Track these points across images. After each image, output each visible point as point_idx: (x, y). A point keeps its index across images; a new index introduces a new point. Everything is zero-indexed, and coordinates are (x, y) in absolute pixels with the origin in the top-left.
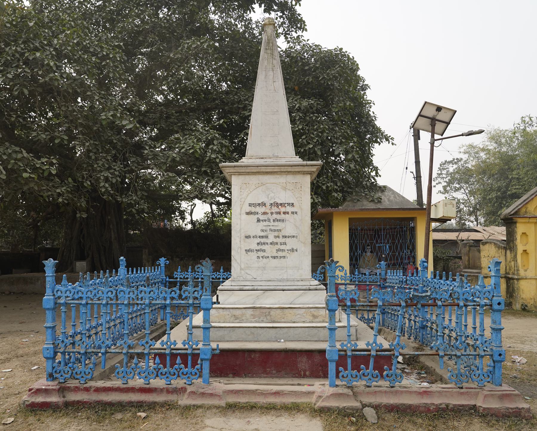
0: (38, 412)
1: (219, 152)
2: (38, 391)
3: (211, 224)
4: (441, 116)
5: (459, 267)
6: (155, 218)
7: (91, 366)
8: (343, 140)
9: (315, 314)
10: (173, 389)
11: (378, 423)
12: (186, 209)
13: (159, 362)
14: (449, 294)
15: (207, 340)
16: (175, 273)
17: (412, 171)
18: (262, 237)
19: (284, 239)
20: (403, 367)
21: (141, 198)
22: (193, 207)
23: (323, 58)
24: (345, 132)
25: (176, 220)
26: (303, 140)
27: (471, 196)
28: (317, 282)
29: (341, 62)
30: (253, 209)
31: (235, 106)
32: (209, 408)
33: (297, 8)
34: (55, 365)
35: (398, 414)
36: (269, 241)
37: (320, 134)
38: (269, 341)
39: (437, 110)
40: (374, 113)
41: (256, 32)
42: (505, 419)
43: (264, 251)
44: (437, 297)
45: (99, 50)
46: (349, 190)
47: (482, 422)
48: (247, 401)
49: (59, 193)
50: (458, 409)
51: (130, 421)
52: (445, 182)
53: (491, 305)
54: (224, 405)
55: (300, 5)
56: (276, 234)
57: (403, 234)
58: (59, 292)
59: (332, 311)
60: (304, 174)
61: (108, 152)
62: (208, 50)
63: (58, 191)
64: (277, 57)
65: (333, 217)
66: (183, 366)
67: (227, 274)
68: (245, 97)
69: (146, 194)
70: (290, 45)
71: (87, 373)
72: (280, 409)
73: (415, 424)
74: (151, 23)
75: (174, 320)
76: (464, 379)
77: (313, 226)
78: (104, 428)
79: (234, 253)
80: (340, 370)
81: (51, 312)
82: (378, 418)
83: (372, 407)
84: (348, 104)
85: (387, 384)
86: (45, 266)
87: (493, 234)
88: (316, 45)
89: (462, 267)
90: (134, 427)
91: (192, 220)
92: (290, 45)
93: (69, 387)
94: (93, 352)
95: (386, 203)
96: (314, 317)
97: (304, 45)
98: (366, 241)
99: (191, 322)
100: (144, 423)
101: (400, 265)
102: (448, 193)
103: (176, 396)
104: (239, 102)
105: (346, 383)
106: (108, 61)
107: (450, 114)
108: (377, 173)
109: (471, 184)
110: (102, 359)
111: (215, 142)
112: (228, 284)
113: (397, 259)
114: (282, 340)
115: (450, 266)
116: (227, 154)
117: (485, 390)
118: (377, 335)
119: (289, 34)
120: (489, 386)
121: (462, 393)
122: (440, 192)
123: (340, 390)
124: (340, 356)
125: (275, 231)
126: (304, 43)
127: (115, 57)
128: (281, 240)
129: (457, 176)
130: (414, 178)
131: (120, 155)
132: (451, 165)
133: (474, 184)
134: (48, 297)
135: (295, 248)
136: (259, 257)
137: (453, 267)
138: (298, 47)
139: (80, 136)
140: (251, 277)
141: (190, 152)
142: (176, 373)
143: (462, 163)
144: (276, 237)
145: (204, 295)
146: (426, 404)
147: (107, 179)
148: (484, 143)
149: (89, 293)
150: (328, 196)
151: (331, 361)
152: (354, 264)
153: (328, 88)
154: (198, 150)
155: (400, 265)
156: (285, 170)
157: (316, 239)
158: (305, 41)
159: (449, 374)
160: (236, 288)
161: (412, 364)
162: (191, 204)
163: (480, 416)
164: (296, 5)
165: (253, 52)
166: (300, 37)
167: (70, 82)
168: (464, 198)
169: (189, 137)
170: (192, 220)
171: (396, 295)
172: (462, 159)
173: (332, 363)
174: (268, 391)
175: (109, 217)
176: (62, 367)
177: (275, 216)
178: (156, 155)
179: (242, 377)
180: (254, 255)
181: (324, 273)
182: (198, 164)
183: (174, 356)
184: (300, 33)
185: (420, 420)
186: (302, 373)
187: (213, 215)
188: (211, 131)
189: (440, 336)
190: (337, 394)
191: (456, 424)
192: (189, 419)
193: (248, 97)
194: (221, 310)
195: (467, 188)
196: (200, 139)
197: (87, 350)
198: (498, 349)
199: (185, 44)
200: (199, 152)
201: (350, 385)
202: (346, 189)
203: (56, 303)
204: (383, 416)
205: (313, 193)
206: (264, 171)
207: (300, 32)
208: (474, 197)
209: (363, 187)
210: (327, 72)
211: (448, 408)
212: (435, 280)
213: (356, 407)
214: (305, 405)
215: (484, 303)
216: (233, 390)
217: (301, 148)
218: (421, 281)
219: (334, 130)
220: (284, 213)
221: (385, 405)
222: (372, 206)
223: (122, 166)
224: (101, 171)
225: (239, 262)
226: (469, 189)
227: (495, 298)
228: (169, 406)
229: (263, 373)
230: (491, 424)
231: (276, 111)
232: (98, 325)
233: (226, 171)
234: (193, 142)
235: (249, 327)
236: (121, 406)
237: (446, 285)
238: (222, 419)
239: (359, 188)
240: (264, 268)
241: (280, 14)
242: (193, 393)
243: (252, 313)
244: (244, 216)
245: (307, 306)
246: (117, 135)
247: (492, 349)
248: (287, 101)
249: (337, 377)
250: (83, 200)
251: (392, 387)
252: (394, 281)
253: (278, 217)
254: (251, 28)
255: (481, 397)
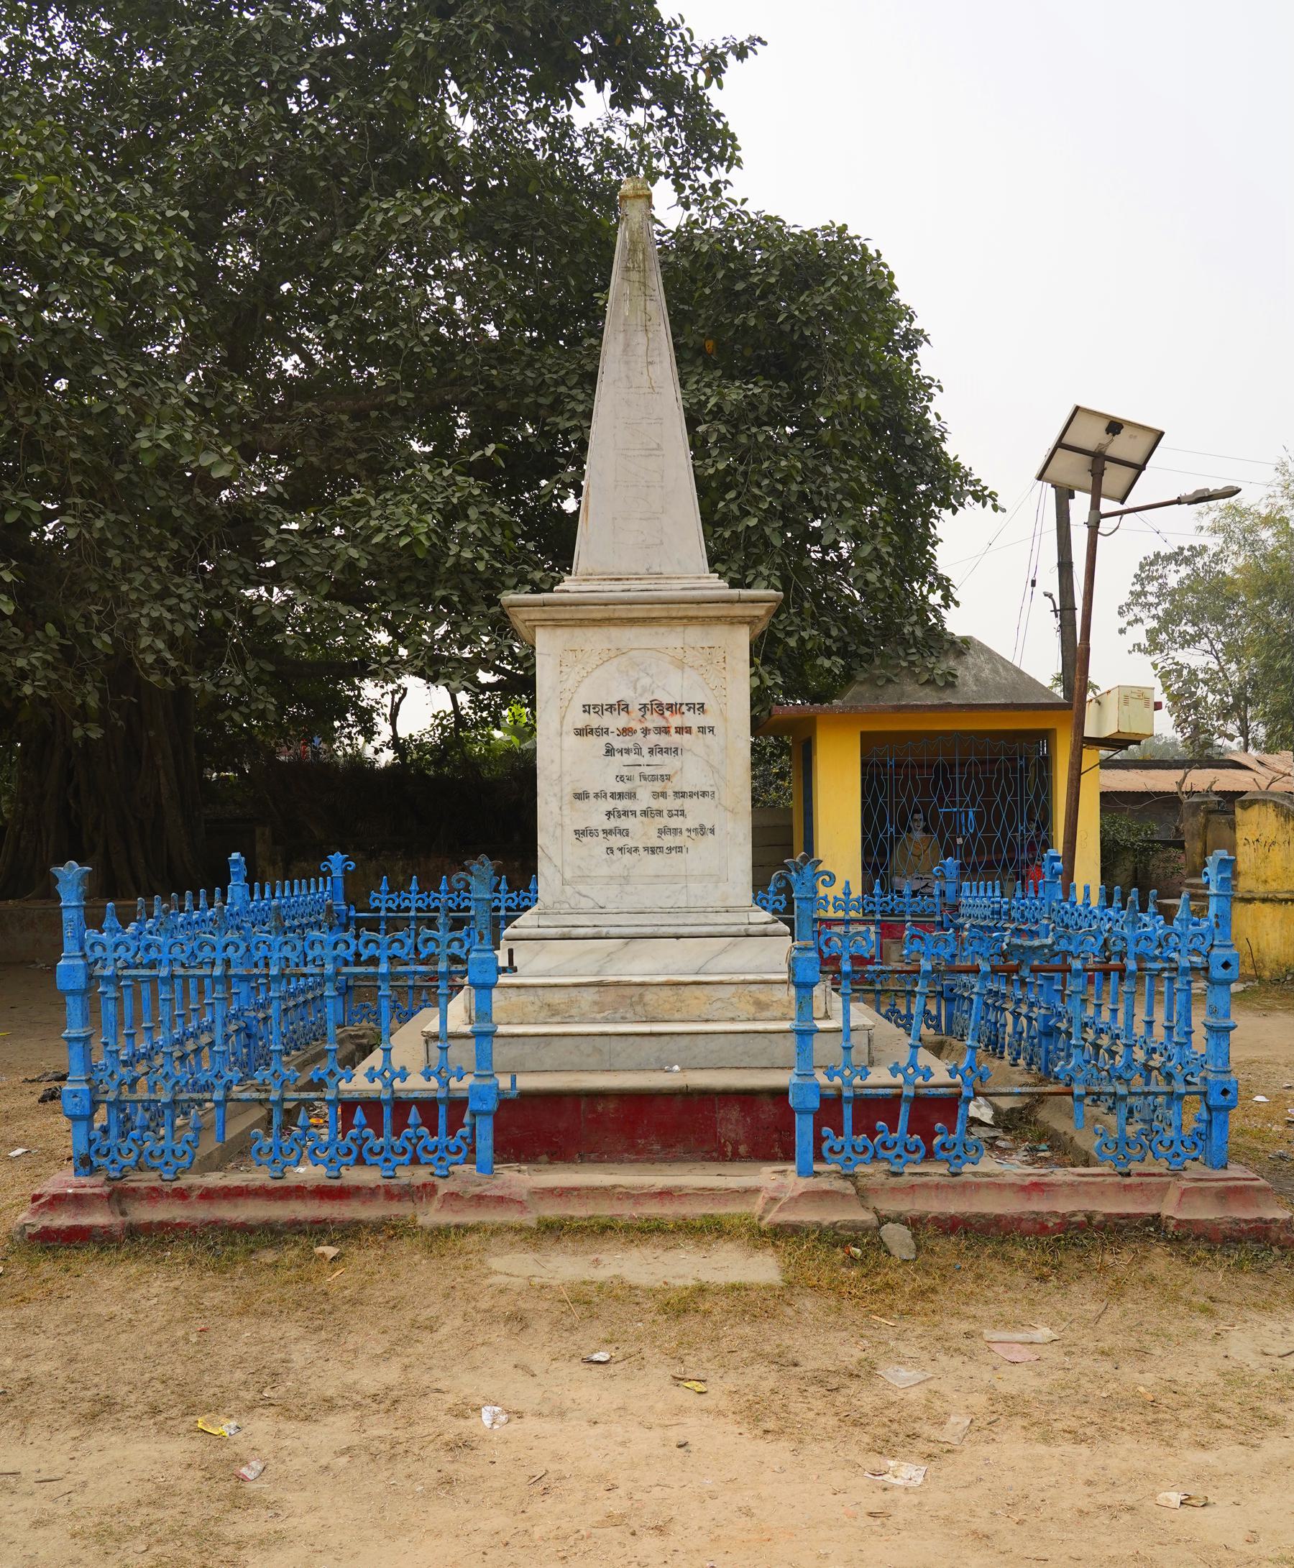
0: (61, 1252)
1: (484, 541)
2: (57, 1201)
3: (452, 748)
4: (1122, 447)
5: (1177, 870)
6: (283, 732)
7: (190, 1135)
8: (847, 504)
9: (762, 997)
10: (403, 1187)
11: (915, 1259)
12: (377, 703)
13: (364, 1121)
14: (1101, 942)
15: (484, 1064)
16: (374, 894)
17: (1049, 591)
18: (621, 795)
19: (679, 801)
20: (992, 1134)
21: (258, 681)
22: (397, 697)
23: (790, 258)
24: (851, 479)
25: (349, 736)
26: (728, 503)
27: (1228, 662)
28: (766, 916)
29: (841, 268)
30: (594, 721)
31: (528, 400)
32: (496, 1231)
33: (712, 93)
34: (96, 1133)
35: (967, 1239)
36: (638, 806)
37: (780, 487)
38: (640, 1069)
39: (1108, 430)
40: (938, 417)
41: (587, 162)
42: (1229, 1248)
43: (624, 833)
44: (1071, 948)
45: (122, 238)
46: (864, 650)
47: (1171, 1255)
48: (590, 1213)
49: (21, 669)
50: (1116, 1224)
51: (299, 1266)
52: (1153, 617)
53: (1206, 969)
54: (533, 1224)
55: (720, 86)
56: (658, 786)
57: (1015, 779)
58: (98, 949)
59: (804, 987)
60: (732, 623)
61: (159, 546)
62: (447, 232)
63: (21, 663)
64: (657, 293)
65: (814, 731)
66: (424, 1130)
67: (399, 896)
68: (556, 372)
69: (271, 668)
70: (691, 215)
71: (178, 1153)
72: (673, 1232)
73: (1008, 1260)
74: (270, 146)
75: (372, 1024)
76: (1135, 1152)
77: (759, 752)
78: (235, 1284)
79: (543, 839)
80: (824, 1134)
81: (79, 999)
82: (918, 1248)
83: (905, 1223)
84: (861, 395)
85: (943, 1169)
86: (57, 881)
87: (1285, 775)
88: (768, 219)
89: (1184, 872)
90: (309, 1280)
91: (395, 736)
92: (691, 215)
93: (134, 1190)
94: (192, 1100)
95: (969, 689)
96: (760, 1005)
97: (731, 215)
98: (910, 799)
99: (443, 1022)
100: (334, 1270)
101: (1005, 868)
102: (1162, 651)
103: (411, 1204)
104: (540, 388)
105: (839, 1168)
106: (150, 272)
107: (1145, 441)
108: (947, 597)
109: (1232, 625)
110: (217, 1114)
111: (473, 513)
112: (530, 923)
113: (999, 850)
114: (676, 1068)
115: (1150, 868)
116: (508, 545)
117: (1184, 1179)
118: (917, 1047)
119: (687, 177)
120: (1195, 1169)
121: (1127, 1188)
122: (1138, 647)
123: (823, 1184)
124: (824, 1100)
125: (654, 778)
126: (734, 209)
127: (169, 258)
128: (671, 803)
129: (1190, 599)
130: (1055, 611)
131: (191, 552)
132: (1173, 567)
133: (1239, 623)
134: (71, 962)
135: (708, 826)
136: (611, 849)
137: (1160, 871)
138: (716, 222)
139: (78, 501)
140: (591, 904)
141: (401, 544)
142: (410, 1148)
143: (1206, 559)
144: (656, 795)
145: (476, 950)
146: (1037, 1213)
147: (157, 627)
148: (1271, 500)
149: (176, 950)
150: (802, 666)
151: (804, 1112)
152: (875, 864)
153: (804, 345)
154: (423, 538)
155: (1005, 868)
156: (681, 614)
157: (766, 791)
158: (735, 203)
159: (1098, 1141)
160: (552, 932)
161: (1016, 1128)
162: (391, 687)
163: (1169, 1241)
164: (708, 84)
165: (578, 235)
166: (721, 186)
167: (41, 338)
168: (1210, 665)
169: (395, 495)
170: (395, 736)
171: (966, 945)
172: (1205, 549)
173: (803, 1116)
174: (642, 1188)
175: (152, 733)
176: (113, 1140)
177: (653, 739)
178: (300, 553)
179: (574, 1162)
180: (597, 846)
181: (788, 890)
182: (422, 578)
183: (401, 1106)
184: (719, 173)
185: (1022, 1253)
186: (729, 1148)
187: (460, 720)
188: (458, 478)
189: (1076, 1046)
190: (818, 1192)
191: (1109, 1259)
192: (447, 1259)
193: (567, 373)
194: (512, 992)
195: (1218, 635)
196: (427, 502)
197: (175, 1094)
198: (1221, 1077)
199: (376, 212)
200: (427, 544)
201: (850, 1172)
202: (854, 647)
203: (90, 977)
204: (930, 1243)
205: (757, 661)
206: (624, 615)
207: (722, 170)
208: (1238, 662)
209: (904, 642)
210: (802, 299)
211: (1090, 1224)
212: (1111, 912)
213: (863, 1222)
214: (736, 1221)
215: (1188, 965)
216: (555, 1189)
217: (725, 527)
218: (1046, 909)
219: (821, 474)
220: (680, 730)
221: (935, 1218)
222: (929, 697)
223: (200, 586)
224: (142, 604)
225: (559, 864)
226: (1223, 639)
227: (1215, 951)
228: (390, 1230)
229: (626, 1151)
230: (1193, 1258)
231: (655, 446)
232: (202, 1029)
233: (519, 619)
234: (408, 514)
235: (588, 1035)
236: (272, 1232)
237: (1106, 919)
238: (530, 1257)
239: (893, 645)
240: (626, 879)
241: (659, 113)
242: (453, 1196)
243: (596, 997)
244: (572, 740)
245: (742, 977)
246: (184, 494)
247: (1205, 1079)
248: (683, 385)
249: (819, 1157)
250: (89, 687)
251: (955, 1175)
252: (977, 912)
253: (663, 741)
254: (571, 150)
255: (1173, 1195)
